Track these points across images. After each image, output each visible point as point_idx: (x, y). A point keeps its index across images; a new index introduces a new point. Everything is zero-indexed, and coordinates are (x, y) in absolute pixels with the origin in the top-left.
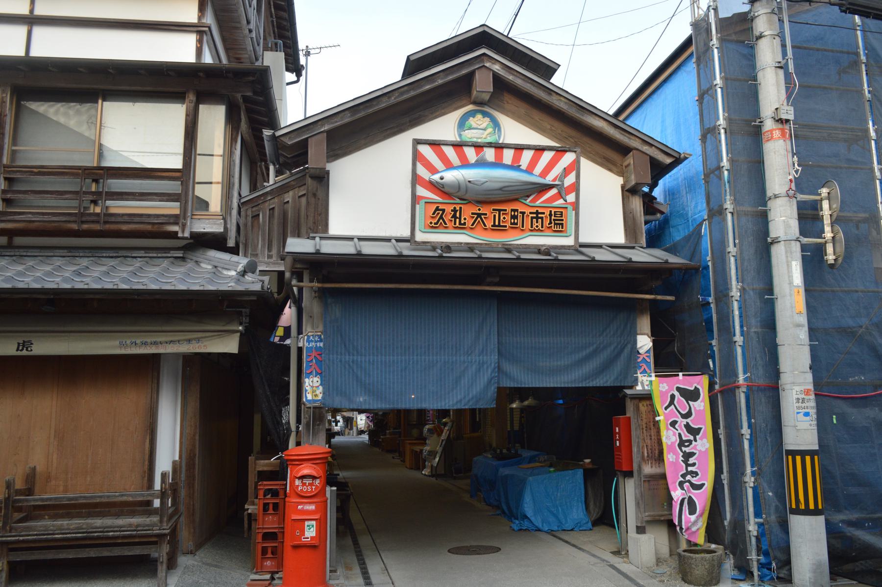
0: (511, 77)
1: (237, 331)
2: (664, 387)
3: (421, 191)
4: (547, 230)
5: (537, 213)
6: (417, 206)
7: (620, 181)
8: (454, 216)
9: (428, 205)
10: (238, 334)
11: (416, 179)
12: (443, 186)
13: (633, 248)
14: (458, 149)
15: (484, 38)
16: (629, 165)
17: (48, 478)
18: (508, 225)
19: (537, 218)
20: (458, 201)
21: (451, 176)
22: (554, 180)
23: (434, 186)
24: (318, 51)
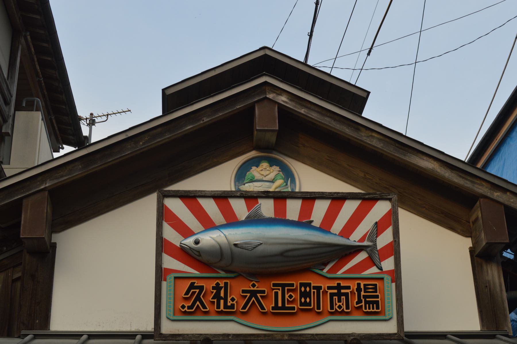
0: (303, 111)
3: (170, 262)
5: (339, 287)
6: (164, 284)
7: (468, 242)
8: (217, 296)
9: (178, 282)
11: (162, 246)
12: (199, 252)
13: (493, 337)
15: (266, 63)
16: (477, 219)
18: (297, 306)
20: (222, 274)
21: (209, 239)
22: (362, 240)
23: (186, 255)
24: (104, 118)
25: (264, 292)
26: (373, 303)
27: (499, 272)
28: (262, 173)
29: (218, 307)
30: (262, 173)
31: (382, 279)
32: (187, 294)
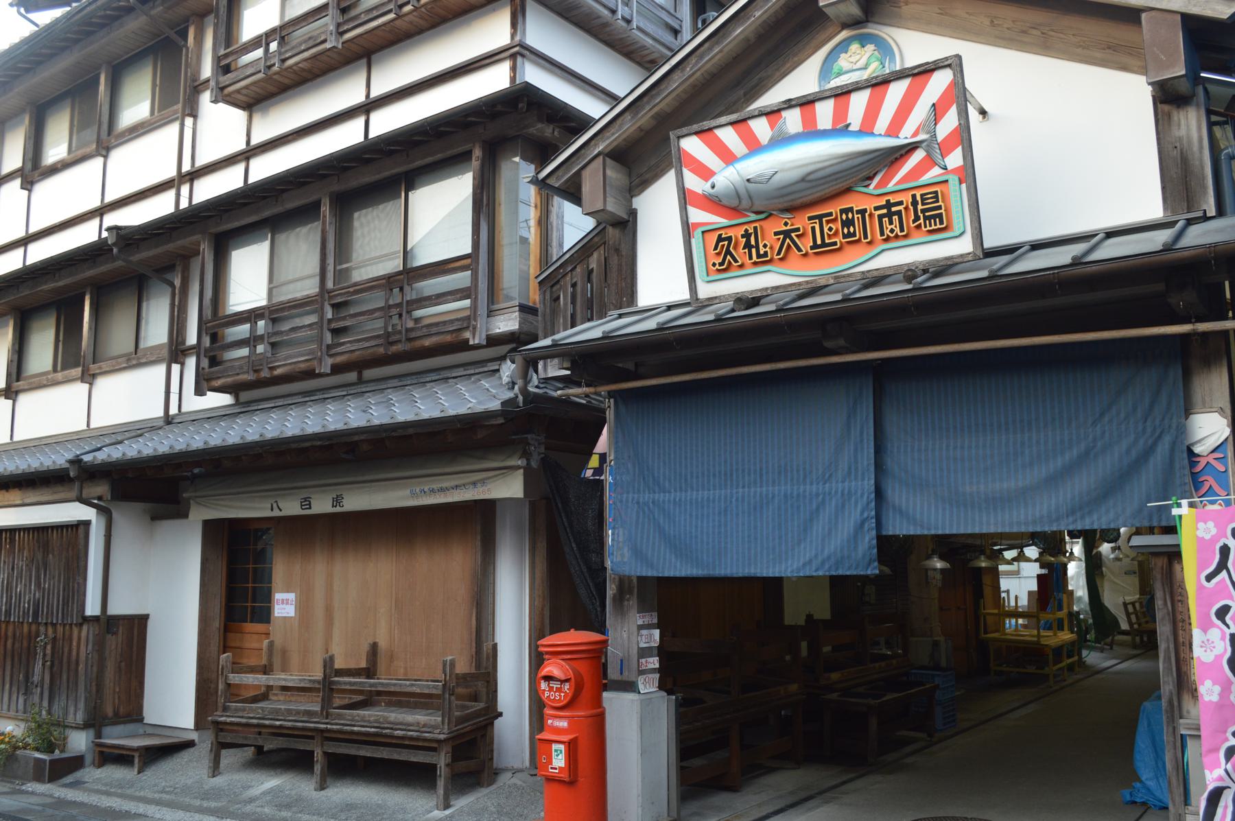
1: (518, 468)
2: (1207, 530)
3: (697, 215)
4: (914, 232)
5: (889, 205)
6: (693, 241)
8: (748, 245)
9: (707, 235)
10: (522, 471)
14: (741, 126)
17: (391, 658)
19: (890, 215)
20: (753, 217)
22: (915, 134)
23: (712, 202)
25: (798, 230)
26: (934, 217)
27: (1199, 121)
28: (852, 59)
29: (751, 258)
30: (852, 59)
31: (946, 181)
32: (716, 248)
